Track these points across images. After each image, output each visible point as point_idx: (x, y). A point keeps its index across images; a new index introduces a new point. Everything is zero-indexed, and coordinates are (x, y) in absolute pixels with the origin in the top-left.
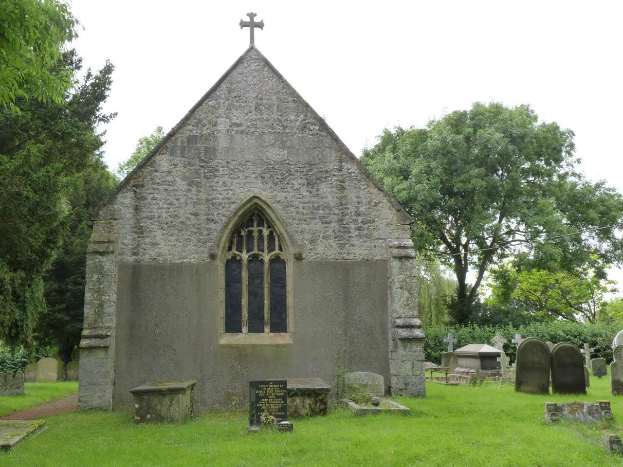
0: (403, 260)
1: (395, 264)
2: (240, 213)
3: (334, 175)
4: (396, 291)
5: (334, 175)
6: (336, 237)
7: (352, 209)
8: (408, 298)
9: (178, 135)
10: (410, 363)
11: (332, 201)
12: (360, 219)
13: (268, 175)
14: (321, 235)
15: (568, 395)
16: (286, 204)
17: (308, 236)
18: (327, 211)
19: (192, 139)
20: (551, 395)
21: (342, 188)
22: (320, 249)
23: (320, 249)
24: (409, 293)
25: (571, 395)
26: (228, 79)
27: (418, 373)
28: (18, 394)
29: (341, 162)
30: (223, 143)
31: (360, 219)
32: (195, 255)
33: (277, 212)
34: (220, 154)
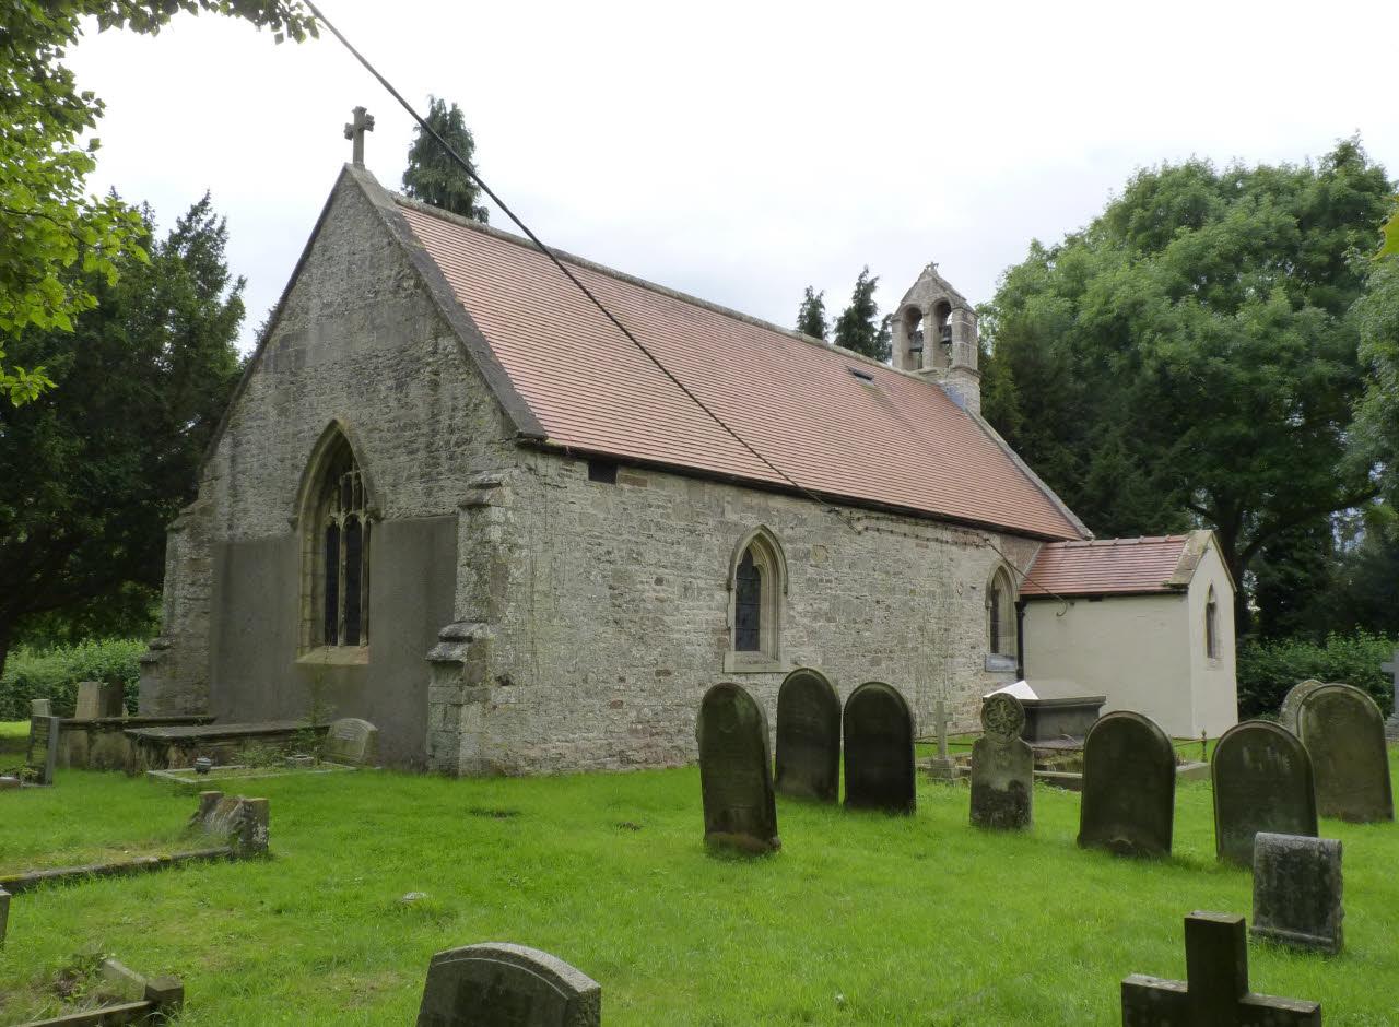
0: (474, 511)
1: (464, 518)
2: (322, 450)
3: (428, 364)
4: (462, 571)
5: (428, 364)
6: (422, 476)
7: (445, 421)
8: (476, 584)
9: (272, 339)
10: (442, 707)
11: (422, 412)
12: (454, 438)
13: (1116, 361)
14: (405, 475)
15: (880, 815)
16: (370, 427)
17: (389, 479)
18: (415, 431)
19: (285, 341)
20: (1187, 866)
21: (435, 385)
22: (403, 501)
23: (403, 501)
24: (477, 574)
25: (866, 816)
26: (322, 232)
27: (450, 726)
28: (1309, 948)
29: (436, 338)
30: (313, 338)
31: (454, 438)
32: (279, 529)
33: (361, 442)
34: (310, 360)
